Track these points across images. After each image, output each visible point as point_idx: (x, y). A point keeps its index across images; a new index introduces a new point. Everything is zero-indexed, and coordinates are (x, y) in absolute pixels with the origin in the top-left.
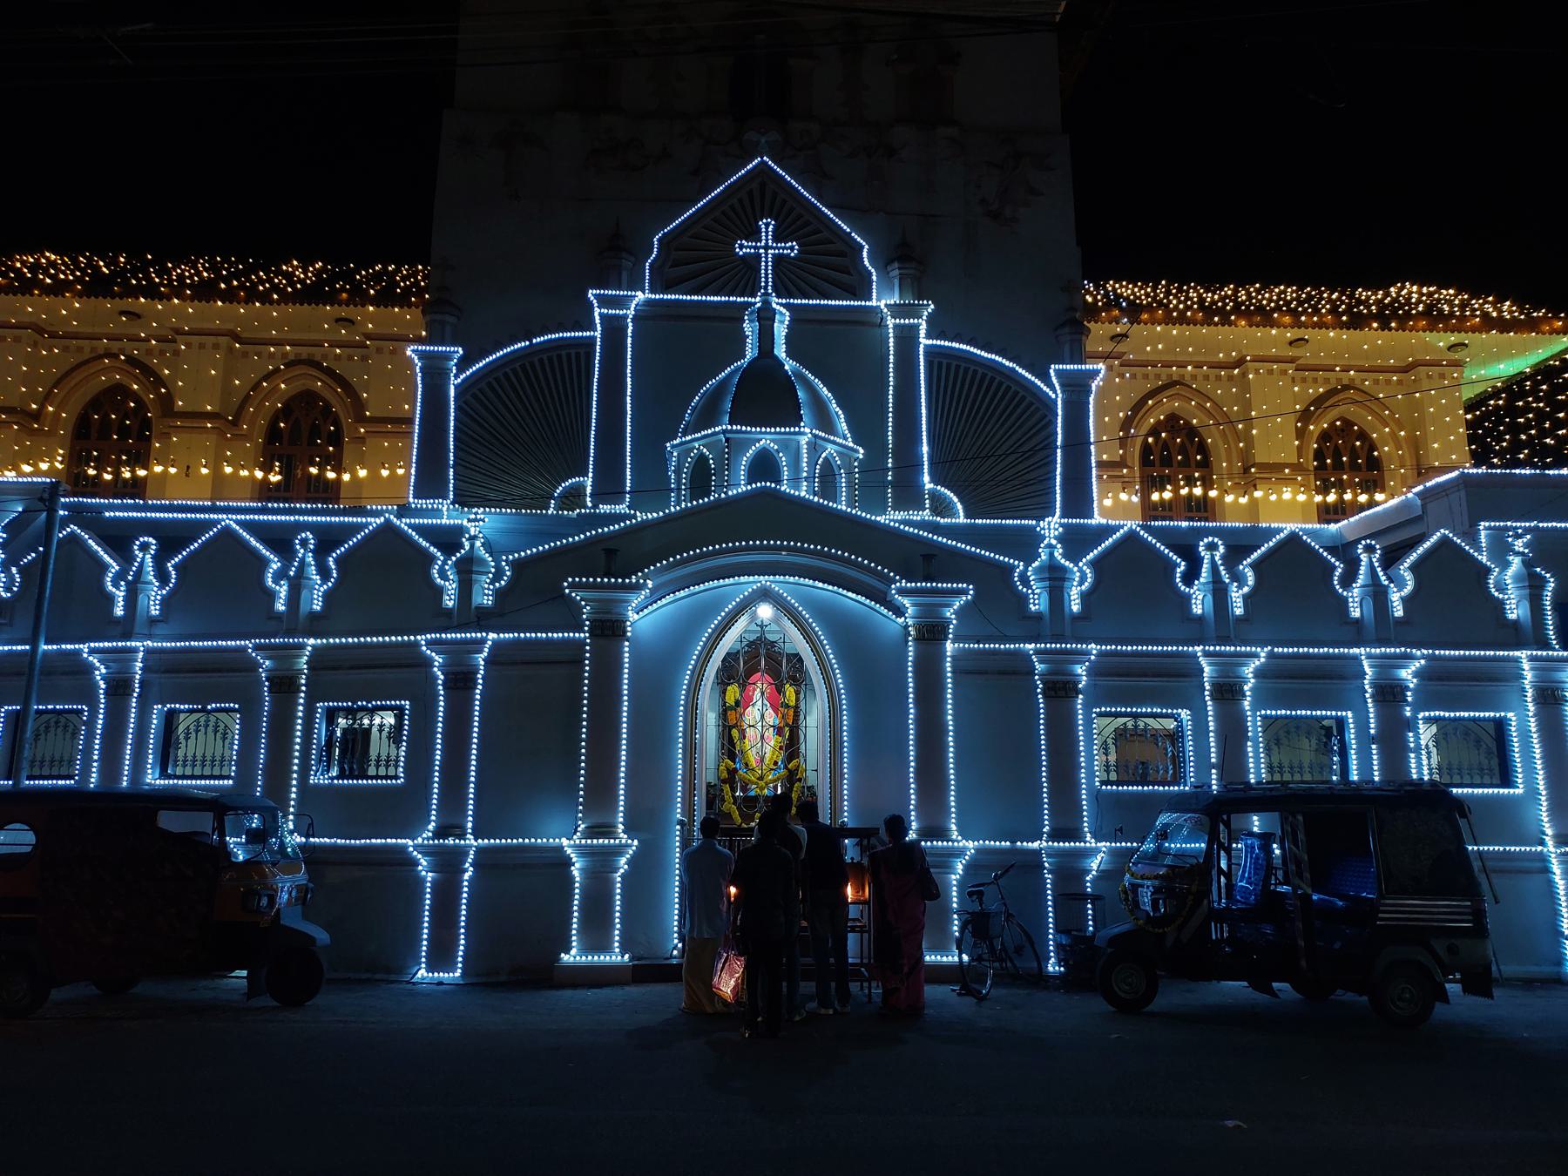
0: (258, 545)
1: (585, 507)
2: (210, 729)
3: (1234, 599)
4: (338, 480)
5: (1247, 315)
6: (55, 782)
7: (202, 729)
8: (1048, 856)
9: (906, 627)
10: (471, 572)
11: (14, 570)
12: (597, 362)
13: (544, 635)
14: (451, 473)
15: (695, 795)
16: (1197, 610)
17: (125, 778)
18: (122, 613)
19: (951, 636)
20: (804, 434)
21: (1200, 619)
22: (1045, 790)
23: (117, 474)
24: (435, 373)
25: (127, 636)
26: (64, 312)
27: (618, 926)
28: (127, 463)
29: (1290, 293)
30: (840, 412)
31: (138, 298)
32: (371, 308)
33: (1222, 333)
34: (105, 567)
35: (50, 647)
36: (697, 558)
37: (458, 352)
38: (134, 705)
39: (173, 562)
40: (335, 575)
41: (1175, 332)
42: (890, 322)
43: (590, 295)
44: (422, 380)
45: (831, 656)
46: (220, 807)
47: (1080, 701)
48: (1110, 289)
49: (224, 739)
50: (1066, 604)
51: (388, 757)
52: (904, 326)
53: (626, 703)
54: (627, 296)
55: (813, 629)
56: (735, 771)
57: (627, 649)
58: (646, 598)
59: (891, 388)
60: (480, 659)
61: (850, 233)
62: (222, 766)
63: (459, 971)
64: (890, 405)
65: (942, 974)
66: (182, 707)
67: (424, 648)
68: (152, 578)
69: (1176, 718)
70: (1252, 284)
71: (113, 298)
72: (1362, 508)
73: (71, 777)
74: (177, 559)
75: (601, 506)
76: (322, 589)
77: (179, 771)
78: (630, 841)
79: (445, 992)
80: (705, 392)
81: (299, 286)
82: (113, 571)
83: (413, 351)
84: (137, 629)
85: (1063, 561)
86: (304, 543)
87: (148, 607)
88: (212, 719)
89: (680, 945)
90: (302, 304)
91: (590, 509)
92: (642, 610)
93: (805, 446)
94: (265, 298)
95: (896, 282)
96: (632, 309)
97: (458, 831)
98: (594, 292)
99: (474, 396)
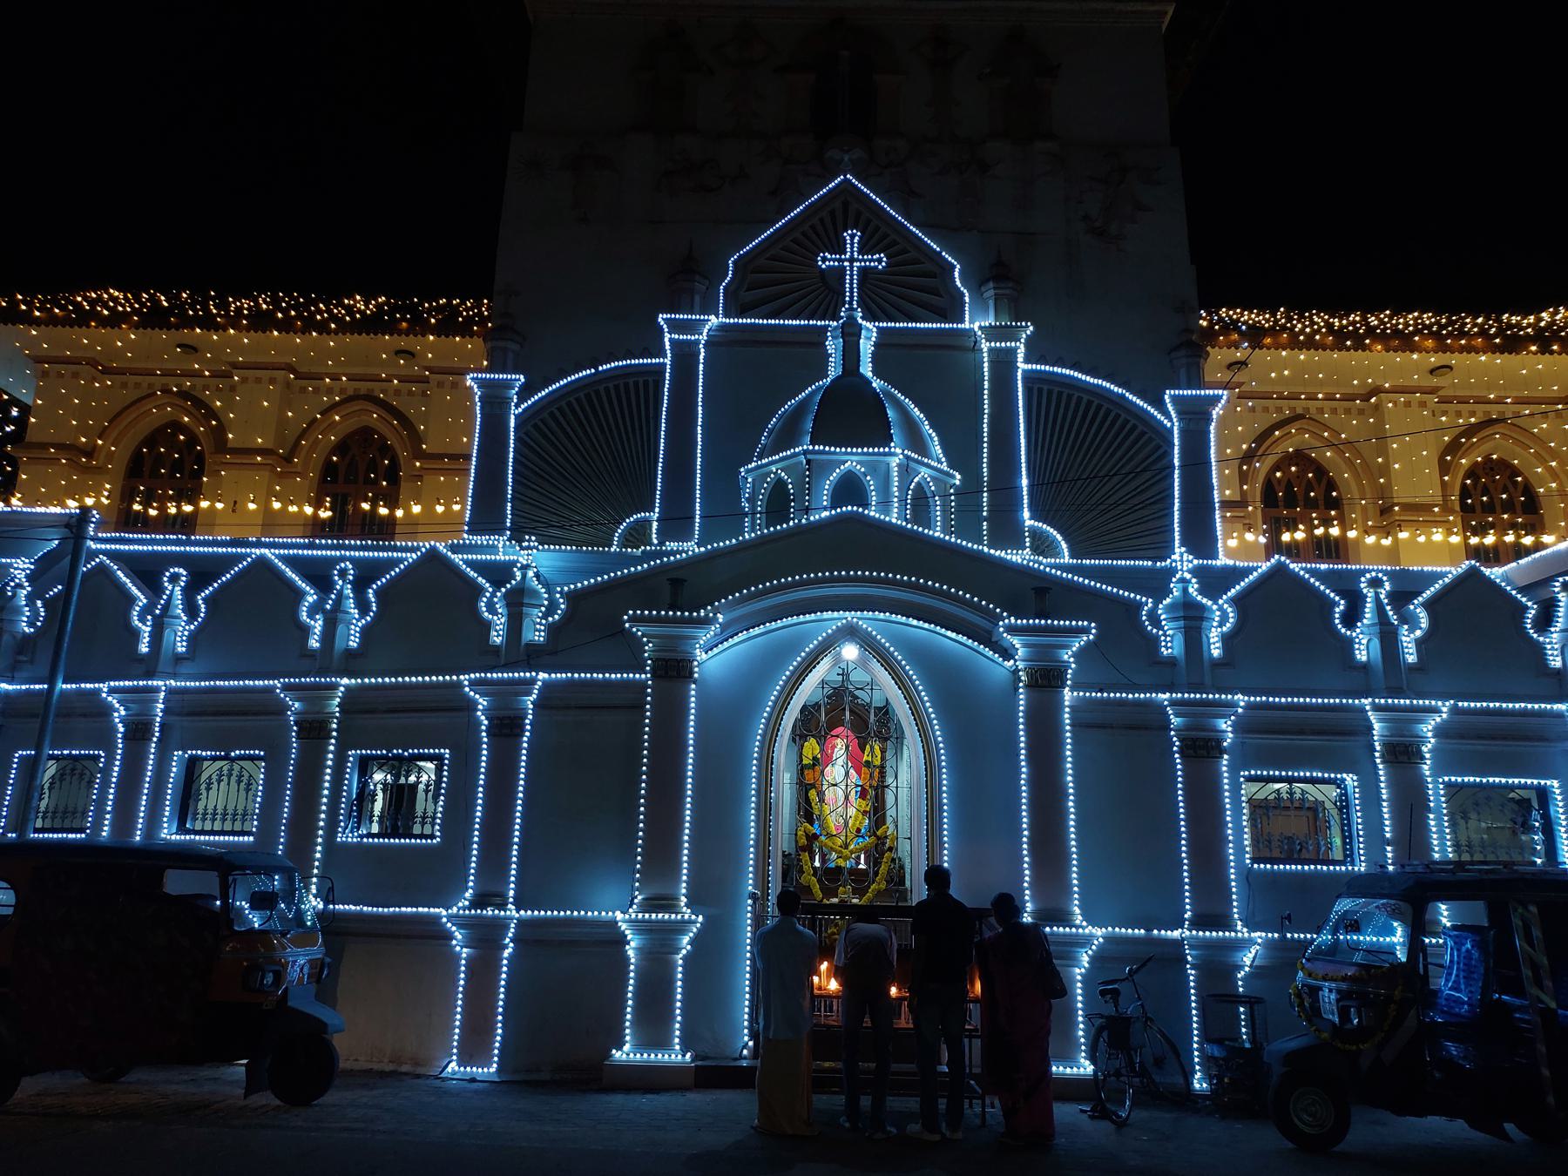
0: (294, 576)
1: (651, 544)
2: (234, 779)
3: (1405, 644)
4: (392, 516)
5: (1383, 338)
6: (65, 835)
7: (225, 778)
8: (1192, 947)
9: (1016, 671)
10: (522, 605)
11: (39, 603)
12: (666, 390)
13: (601, 676)
14: (509, 508)
15: (769, 865)
16: (1361, 656)
17: (139, 833)
18: (147, 649)
19: (1069, 682)
20: (894, 454)
21: (1365, 667)
22: (1185, 867)
23: (162, 509)
24: (495, 402)
25: (150, 675)
26: (119, 344)
27: (679, 1018)
28: (171, 499)
29: (1428, 318)
30: (934, 434)
31: (194, 329)
32: (431, 338)
33: (1355, 358)
34: (132, 600)
35: (69, 686)
36: (774, 590)
37: (519, 380)
38: (153, 750)
39: (203, 594)
40: (374, 609)
41: (1302, 357)
42: (985, 346)
43: (660, 320)
44: (482, 408)
45: (928, 704)
46: (225, 865)
47: (1225, 762)
48: (1224, 315)
49: (248, 790)
50: (1205, 648)
51: (425, 813)
52: (1000, 350)
53: (691, 755)
54: (700, 320)
55: (906, 673)
56: (815, 837)
57: (693, 693)
58: (715, 635)
59: (986, 416)
60: (529, 702)
61: (941, 253)
62: (243, 821)
63: (495, 1065)
64: (985, 434)
65: (1074, 1089)
66: (204, 753)
67: (467, 689)
68: (180, 611)
69: (1339, 784)
70: (1382, 311)
71: (169, 329)
72: (1528, 551)
73: (81, 831)
74: (207, 592)
75: (667, 543)
76: (360, 624)
77: (198, 827)
78: (693, 917)
79: (476, 1092)
80: (784, 413)
81: (358, 316)
82: (141, 604)
83: (473, 379)
84: (160, 668)
85: (1199, 598)
86: (343, 573)
87: (175, 644)
88: (237, 768)
89: (751, 1043)
90: (360, 334)
91: (656, 546)
92: (711, 649)
93: (896, 469)
94: (322, 328)
95: (991, 303)
96: (705, 334)
97: (498, 900)
98: (665, 316)
99: (535, 426)
